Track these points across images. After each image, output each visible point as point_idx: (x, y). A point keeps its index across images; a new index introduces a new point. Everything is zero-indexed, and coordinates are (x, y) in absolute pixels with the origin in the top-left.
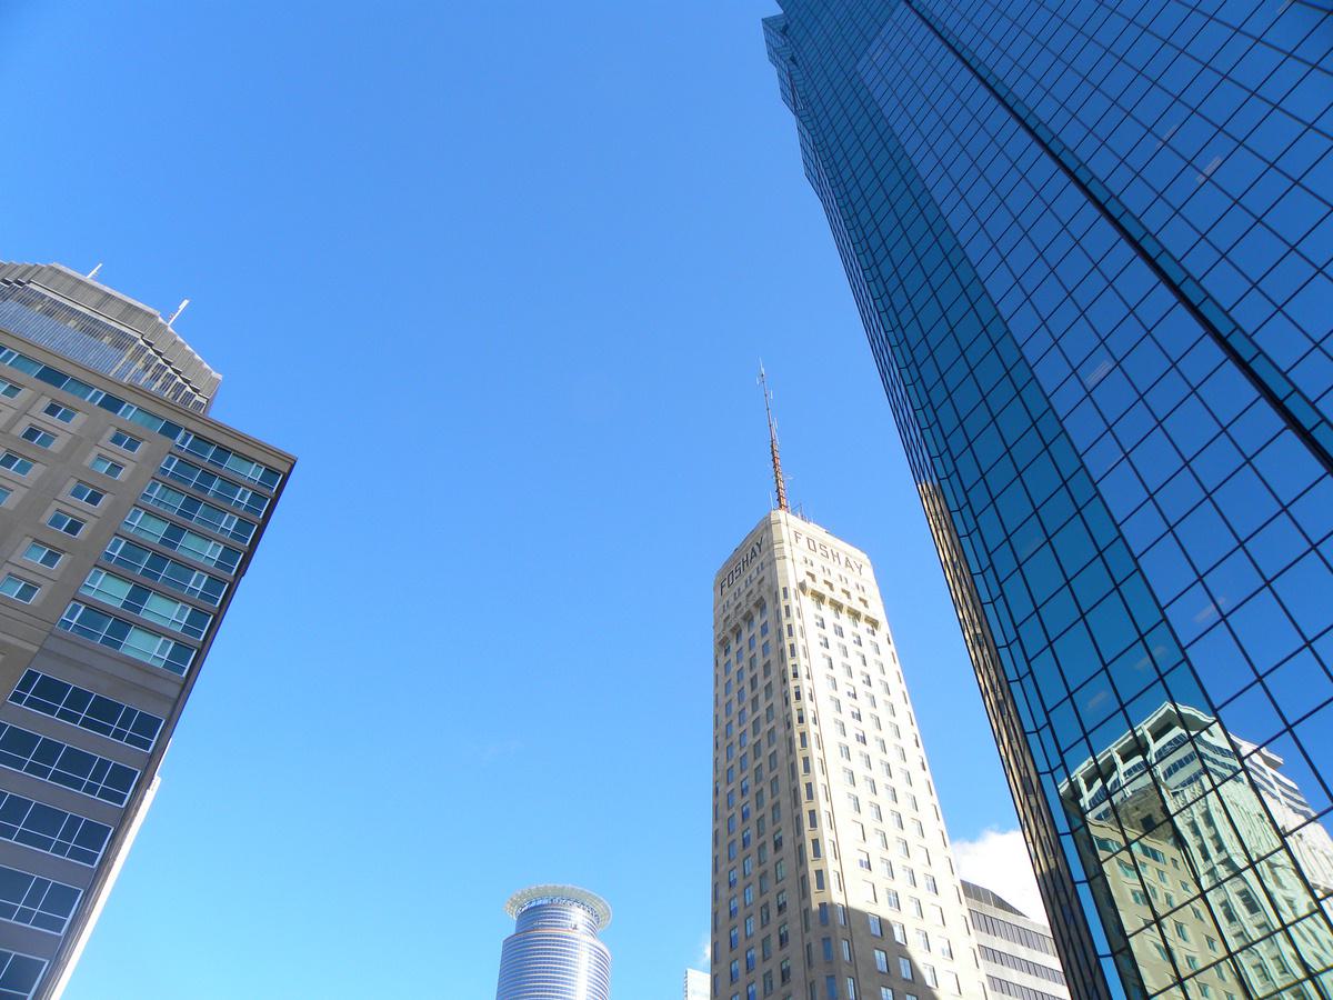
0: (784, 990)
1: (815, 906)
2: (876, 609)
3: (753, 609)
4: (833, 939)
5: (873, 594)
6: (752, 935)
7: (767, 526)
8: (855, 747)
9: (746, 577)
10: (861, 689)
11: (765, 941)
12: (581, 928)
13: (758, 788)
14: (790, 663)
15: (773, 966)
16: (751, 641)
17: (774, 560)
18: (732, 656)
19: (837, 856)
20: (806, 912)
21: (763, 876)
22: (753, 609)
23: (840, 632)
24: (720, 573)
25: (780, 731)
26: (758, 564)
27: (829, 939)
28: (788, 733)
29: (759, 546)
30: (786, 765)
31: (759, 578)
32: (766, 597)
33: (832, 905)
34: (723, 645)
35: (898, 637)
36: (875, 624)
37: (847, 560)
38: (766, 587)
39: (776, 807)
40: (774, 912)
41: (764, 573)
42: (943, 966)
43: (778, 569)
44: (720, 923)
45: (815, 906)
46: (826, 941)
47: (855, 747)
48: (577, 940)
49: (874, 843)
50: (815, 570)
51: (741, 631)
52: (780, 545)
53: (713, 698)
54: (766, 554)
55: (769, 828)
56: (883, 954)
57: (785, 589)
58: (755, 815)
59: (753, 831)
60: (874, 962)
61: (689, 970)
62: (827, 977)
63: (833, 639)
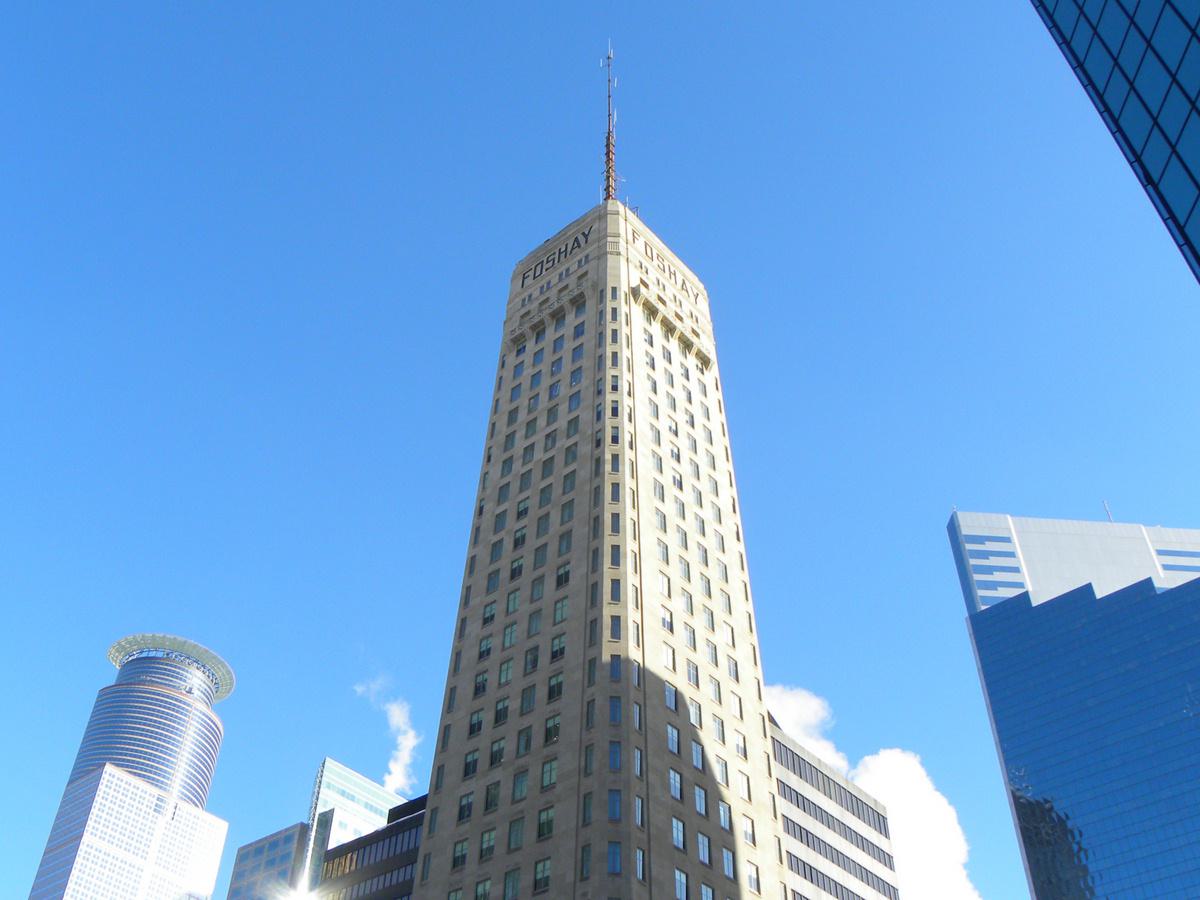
0: (546, 751)
1: (606, 658)
2: (707, 344)
3: (548, 320)
4: (623, 700)
5: (706, 325)
6: (507, 683)
7: (602, 215)
8: (671, 491)
9: (563, 269)
10: (684, 428)
11: (528, 693)
12: (196, 692)
13: (542, 512)
14: (610, 372)
15: (536, 722)
16: (558, 343)
17: (606, 253)
18: (527, 358)
19: (639, 605)
20: (593, 663)
21: (535, 615)
22: (548, 320)
23: (668, 357)
24: (534, 255)
25: (585, 449)
26: (581, 256)
27: (619, 698)
28: (597, 452)
29: (586, 236)
30: (587, 488)
31: (580, 273)
32: (588, 293)
33: (628, 660)
34: (517, 343)
35: (726, 383)
36: (705, 362)
37: (684, 282)
38: (590, 284)
39: (566, 537)
40: (544, 659)
41: (590, 267)
42: (735, 764)
43: (609, 264)
44: (464, 663)
45: (606, 658)
46: (615, 701)
47: (671, 491)
48: (189, 705)
49: (678, 604)
50: (651, 280)
51: (544, 330)
52: (615, 239)
53: (490, 404)
54: (595, 246)
55: (552, 557)
56: (675, 732)
57: (614, 290)
58: (532, 543)
59: (528, 561)
60: (666, 739)
61: (328, 759)
62: (611, 742)
63: (660, 363)
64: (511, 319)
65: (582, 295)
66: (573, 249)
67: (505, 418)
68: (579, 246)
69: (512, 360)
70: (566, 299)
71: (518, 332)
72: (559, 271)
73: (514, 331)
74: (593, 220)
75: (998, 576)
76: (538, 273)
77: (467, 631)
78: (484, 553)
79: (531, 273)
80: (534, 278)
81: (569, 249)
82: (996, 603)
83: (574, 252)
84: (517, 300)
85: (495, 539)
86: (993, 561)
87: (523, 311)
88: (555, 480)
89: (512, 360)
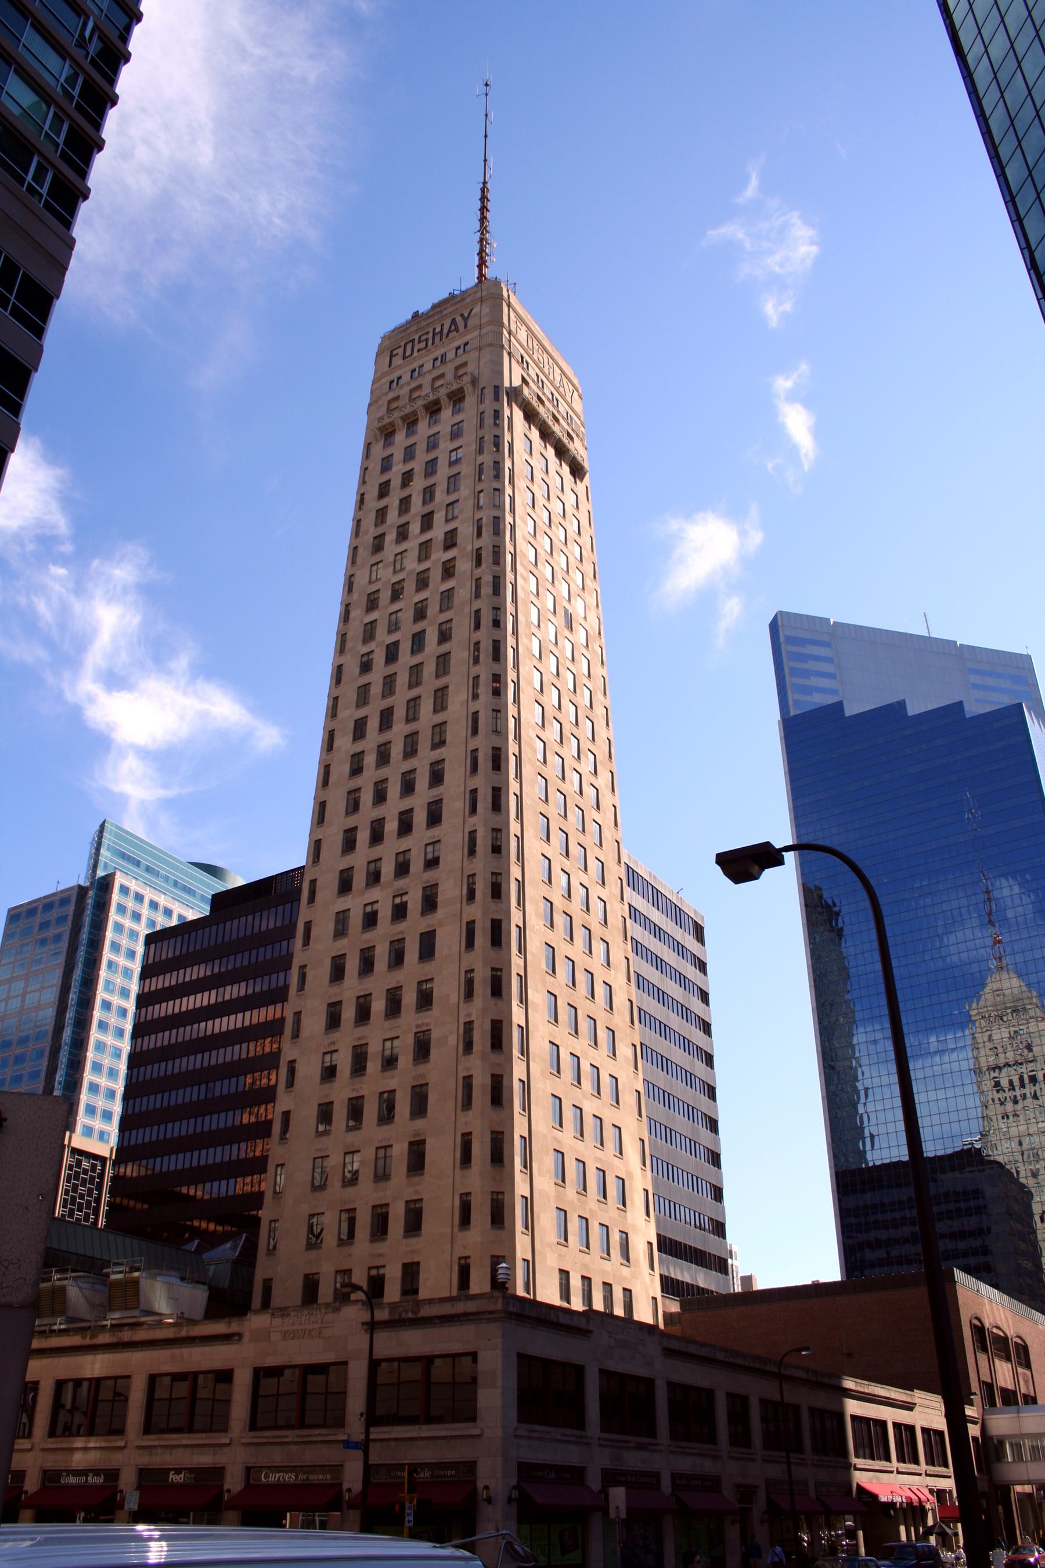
26: (460, 342)
29: (466, 320)
30: (467, 610)
32: (468, 390)
54: (476, 333)
62: (493, 873)
64: (377, 401)
65: (461, 390)
66: (449, 331)
67: (372, 516)
68: (457, 330)
69: (379, 451)
70: (443, 392)
71: (386, 421)
72: (433, 356)
73: (382, 418)
74: (474, 303)
75: (814, 681)
76: (409, 346)
77: (336, 744)
78: (352, 667)
79: (400, 351)
80: (404, 358)
81: (445, 331)
82: (813, 708)
83: (451, 335)
84: (383, 381)
85: (365, 649)
86: (811, 665)
87: (391, 396)
88: (432, 595)
89: (379, 451)
